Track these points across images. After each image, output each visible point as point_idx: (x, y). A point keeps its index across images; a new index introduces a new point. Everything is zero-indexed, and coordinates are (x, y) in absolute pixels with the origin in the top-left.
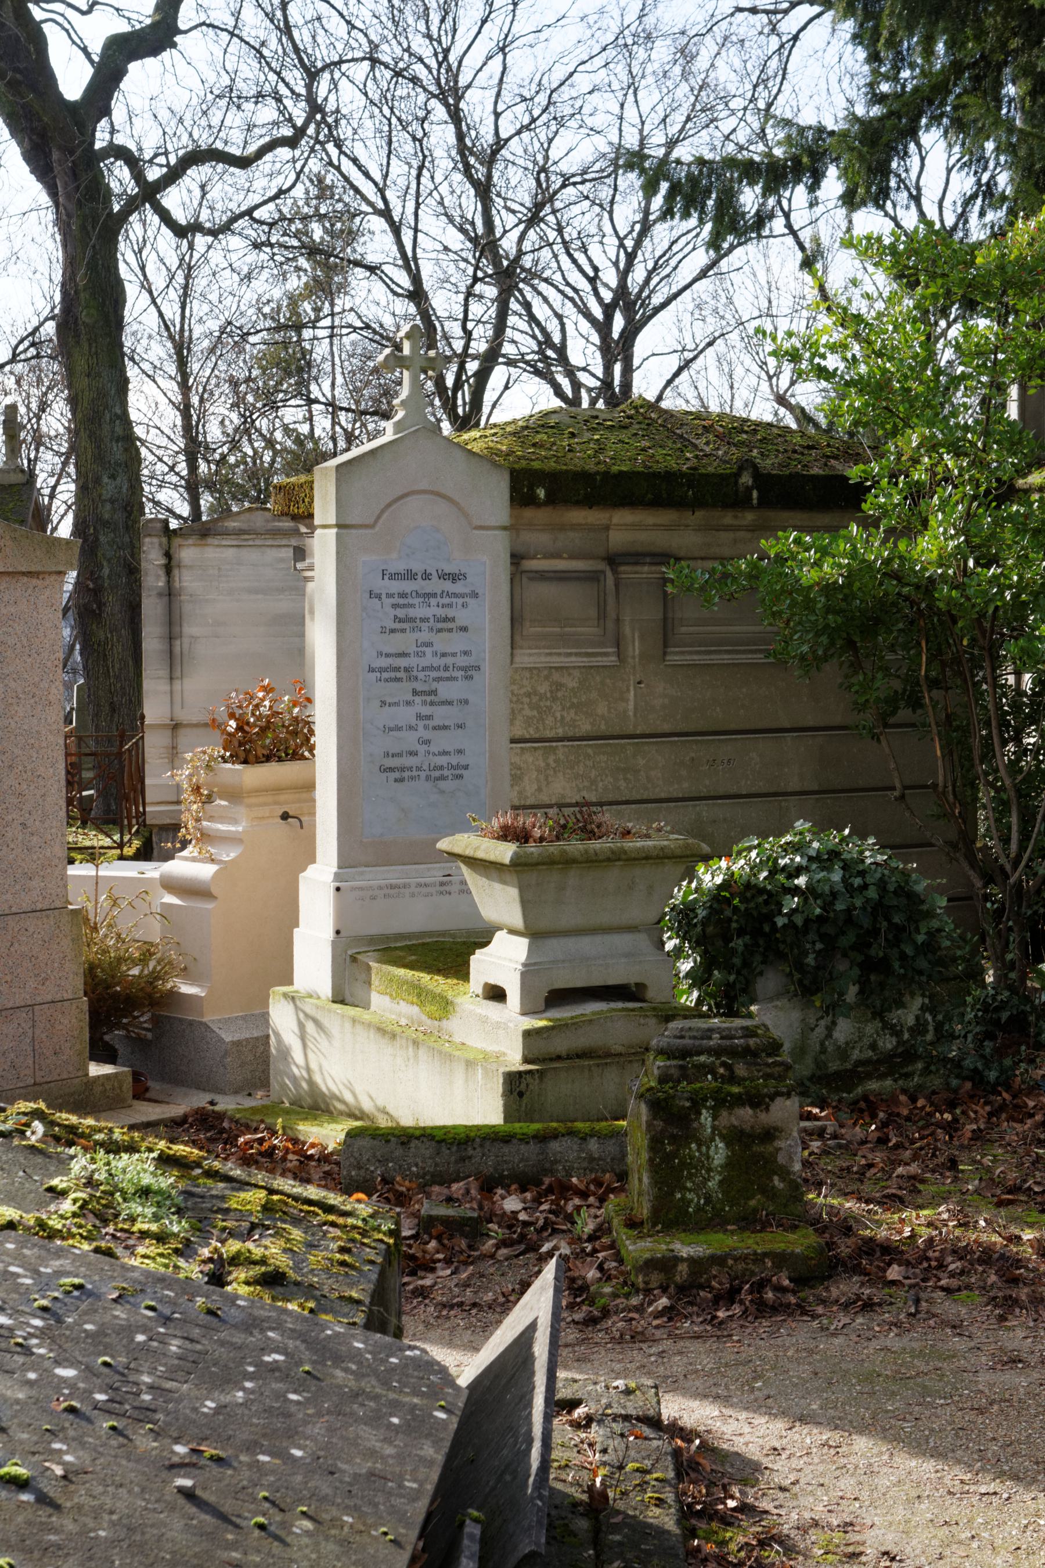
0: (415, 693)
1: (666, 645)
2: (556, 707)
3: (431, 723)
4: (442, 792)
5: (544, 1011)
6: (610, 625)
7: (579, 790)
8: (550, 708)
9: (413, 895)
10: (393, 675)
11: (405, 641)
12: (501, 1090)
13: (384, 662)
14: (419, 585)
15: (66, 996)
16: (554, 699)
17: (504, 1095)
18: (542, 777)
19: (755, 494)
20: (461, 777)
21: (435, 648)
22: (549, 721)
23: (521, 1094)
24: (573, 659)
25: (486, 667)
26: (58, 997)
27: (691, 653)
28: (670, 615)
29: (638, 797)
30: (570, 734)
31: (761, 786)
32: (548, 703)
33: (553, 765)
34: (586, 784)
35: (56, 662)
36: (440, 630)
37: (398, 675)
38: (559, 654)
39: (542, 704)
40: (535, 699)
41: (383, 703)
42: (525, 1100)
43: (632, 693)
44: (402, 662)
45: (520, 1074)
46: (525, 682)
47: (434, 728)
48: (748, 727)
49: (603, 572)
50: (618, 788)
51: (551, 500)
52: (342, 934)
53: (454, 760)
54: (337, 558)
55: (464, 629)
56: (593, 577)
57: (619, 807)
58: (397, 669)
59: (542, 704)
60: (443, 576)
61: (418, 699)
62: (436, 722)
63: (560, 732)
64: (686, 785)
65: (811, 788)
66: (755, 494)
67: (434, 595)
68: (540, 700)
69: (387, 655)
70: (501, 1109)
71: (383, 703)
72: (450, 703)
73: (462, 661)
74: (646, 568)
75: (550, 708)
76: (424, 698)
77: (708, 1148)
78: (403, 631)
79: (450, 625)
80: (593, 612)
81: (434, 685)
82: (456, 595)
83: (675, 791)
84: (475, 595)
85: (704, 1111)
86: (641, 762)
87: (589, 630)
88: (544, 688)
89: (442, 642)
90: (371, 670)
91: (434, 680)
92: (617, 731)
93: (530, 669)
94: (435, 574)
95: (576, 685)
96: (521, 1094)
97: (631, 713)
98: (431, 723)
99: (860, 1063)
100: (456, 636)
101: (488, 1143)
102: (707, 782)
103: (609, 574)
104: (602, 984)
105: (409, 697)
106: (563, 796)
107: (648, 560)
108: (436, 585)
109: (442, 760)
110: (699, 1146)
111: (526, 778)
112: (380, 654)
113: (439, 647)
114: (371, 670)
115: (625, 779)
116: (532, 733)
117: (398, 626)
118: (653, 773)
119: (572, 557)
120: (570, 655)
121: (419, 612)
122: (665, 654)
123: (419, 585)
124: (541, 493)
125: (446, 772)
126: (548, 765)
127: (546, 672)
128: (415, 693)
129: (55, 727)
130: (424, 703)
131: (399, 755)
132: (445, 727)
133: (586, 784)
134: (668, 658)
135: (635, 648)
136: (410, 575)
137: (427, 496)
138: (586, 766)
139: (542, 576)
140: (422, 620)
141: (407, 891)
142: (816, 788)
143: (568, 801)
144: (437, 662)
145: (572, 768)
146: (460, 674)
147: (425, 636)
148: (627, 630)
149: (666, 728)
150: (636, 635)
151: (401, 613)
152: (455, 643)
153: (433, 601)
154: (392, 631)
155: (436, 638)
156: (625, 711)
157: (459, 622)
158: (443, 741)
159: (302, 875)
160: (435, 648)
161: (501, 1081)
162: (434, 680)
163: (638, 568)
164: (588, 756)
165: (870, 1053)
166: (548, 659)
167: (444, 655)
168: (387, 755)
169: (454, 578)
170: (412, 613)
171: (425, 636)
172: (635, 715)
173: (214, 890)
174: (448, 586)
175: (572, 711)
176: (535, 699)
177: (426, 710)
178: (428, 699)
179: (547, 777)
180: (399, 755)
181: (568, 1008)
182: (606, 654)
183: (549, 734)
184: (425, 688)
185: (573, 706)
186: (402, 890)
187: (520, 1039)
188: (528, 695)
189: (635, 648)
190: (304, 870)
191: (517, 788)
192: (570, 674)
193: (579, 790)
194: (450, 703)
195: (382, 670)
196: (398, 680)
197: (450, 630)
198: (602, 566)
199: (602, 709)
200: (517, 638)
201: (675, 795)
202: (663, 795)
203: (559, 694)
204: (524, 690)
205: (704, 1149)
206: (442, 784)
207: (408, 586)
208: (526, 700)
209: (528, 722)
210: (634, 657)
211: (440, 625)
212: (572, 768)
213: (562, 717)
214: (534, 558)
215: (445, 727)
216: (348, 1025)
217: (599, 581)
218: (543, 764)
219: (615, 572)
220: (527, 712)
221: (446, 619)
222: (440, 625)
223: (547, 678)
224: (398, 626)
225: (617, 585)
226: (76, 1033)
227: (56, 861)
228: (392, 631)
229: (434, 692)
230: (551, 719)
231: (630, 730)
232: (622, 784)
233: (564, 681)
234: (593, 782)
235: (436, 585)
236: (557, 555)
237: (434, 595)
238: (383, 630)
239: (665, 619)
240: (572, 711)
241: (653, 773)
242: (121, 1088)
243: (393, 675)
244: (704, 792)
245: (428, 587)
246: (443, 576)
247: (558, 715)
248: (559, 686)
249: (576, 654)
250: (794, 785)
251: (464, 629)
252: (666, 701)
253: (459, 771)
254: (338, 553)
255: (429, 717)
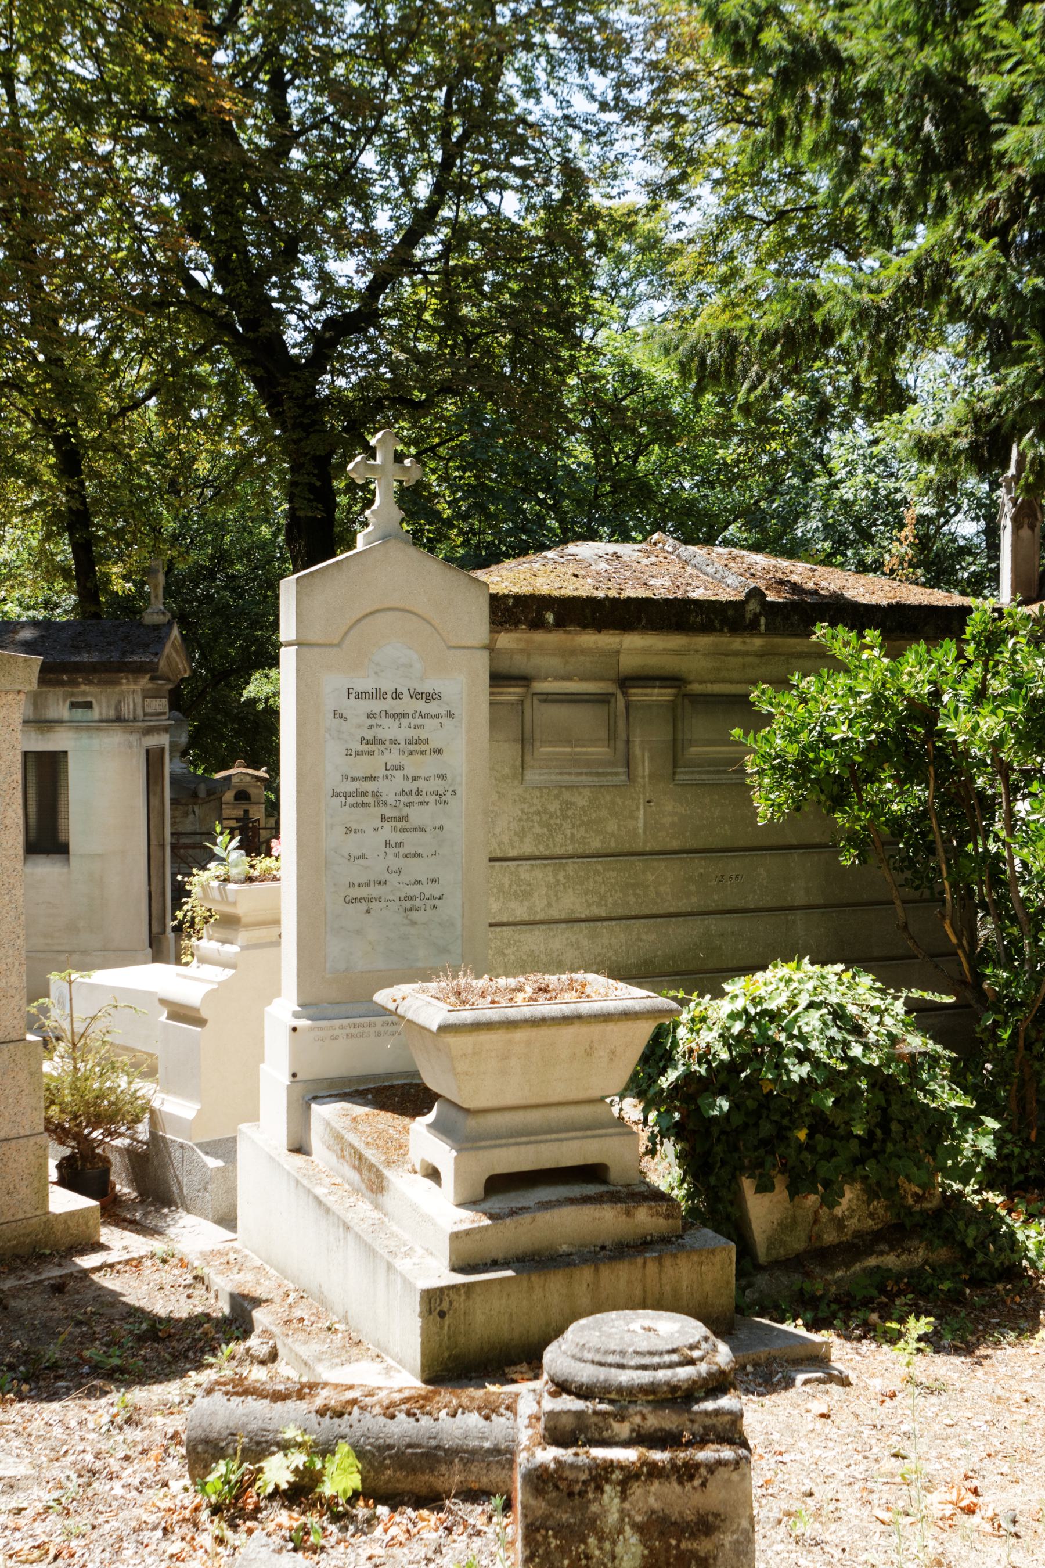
0: (384, 819)
1: (675, 765)
2: (567, 825)
3: (402, 851)
4: (413, 923)
5: (484, 1200)
6: (621, 745)
7: (589, 906)
8: (560, 826)
9: (379, 1034)
10: (359, 800)
11: (373, 764)
12: (418, 1309)
13: (350, 786)
14: (389, 705)
15: (22, 1133)
16: (565, 817)
17: (422, 1315)
18: (551, 893)
19: (763, 620)
20: (435, 907)
21: (405, 772)
22: (559, 838)
23: (442, 1314)
24: (584, 778)
25: (462, 791)
26: (13, 1134)
27: (699, 773)
28: (680, 736)
29: (648, 912)
30: (580, 851)
31: (768, 901)
32: (558, 821)
33: (563, 881)
34: (596, 899)
35: (14, 785)
36: (412, 753)
37: (366, 800)
38: (570, 774)
39: (552, 822)
40: (545, 817)
41: (349, 830)
42: (447, 1320)
43: (642, 812)
44: (369, 786)
45: (441, 1291)
46: (535, 801)
47: (405, 856)
48: (756, 844)
49: (614, 694)
50: (628, 903)
51: (560, 624)
52: (297, 1079)
53: (428, 890)
54: (297, 677)
55: (438, 751)
56: (603, 700)
57: (628, 922)
58: (364, 794)
59: (552, 822)
60: (415, 695)
61: (387, 826)
62: (407, 850)
63: (570, 849)
64: (694, 900)
65: (817, 902)
66: (763, 620)
67: (406, 715)
68: (551, 817)
69: (353, 779)
70: (418, 1331)
71: (349, 830)
72: (421, 829)
73: (437, 785)
74: (656, 691)
75: (560, 826)
76: (394, 824)
77: (614, 1543)
78: (371, 753)
79: (423, 747)
80: (603, 734)
81: (406, 811)
82: (429, 716)
83: (683, 905)
84: (451, 715)
85: (607, 1488)
86: (651, 878)
87: (599, 751)
88: (554, 807)
89: (413, 765)
90: (336, 794)
91: (405, 805)
92: (626, 847)
93: (540, 788)
94: (406, 693)
95: (586, 804)
96: (442, 1314)
97: (641, 831)
98: (402, 851)
99: (858, 1234)
100: (429, 758)
101: (836, 789)
102: (716, 897)
103: (620, 696)
104: (553, 1166)
105: (378, 823)
106: (573, 912)
107: (658, 683)
108: (408, 705)
109: (415, 890)
110: (601, 1539)
111: (536, 895)
112: (345, 777)
113: (410, 771)
114: (336, 794)
115: (635, 894)
116: (542, 850)
117: (364, 747)
118: (662, 889)
119: (583, 679)
120: (581, 774)
121: (390, 730)
122: (674, 773)
123: (389, 705)
124: (550, 617)
125: (417, 903)
126: (558, 881)
127: (556, 792)
128: (384, 819)
129: (12, 852)
130: (394, 829)
131: (367, 884)
132: (417, 855)
133: (596, 899)
134: (677, 777)
135: (644, 767)
136: (379, 695)
137: (397, 613)
138: (596, 882)
139: (548, 698)
140: (393, 742)
141: (372, 1030)
142: (822, 902)
143: (578, 915)
144: (408, 786)
145: (582, 884)
146: (432, 799)
147: (394, 757)
148: (637, 751)
149: (675, 844)
150: (647, 755)
151: (369, 735)
152: (428, 766)
153: (405, 722)
154: (359, 753)
155: (409, 762)
156: (635, 829)
157: (433, 744)
158: (416, 869)
159: (267, 1009)
160: (405, 772)
161: (418, 1299)
162: (405, 805)
163: (648, 691)
164: (597, 872)
165: (870, 1222)
166: (559, 777)
167: (416, 778)
168: (352, 885)
169: (429, 697)
170: (381, 734)
171: (394, 757)
172: (645, 832)
173: (204, 1014)
174: (421, 705)
175: (583, 829)
176: (545, 817)
177: (398, 837)
178: (399, 825)
179: (557, 892)
180: (367, 884)
181: (513, 1195)
182: (616, 774)
183: (559, 851)
184: (395, 813)
185: (583, 823)
186: (367, 1029)
187: (447, 1241)
188: (538, 813)
189: (644, 767)
190: (269, 1003)
191: (526, 904)
192: (580, 794)
193: (589, 906)
194: (421, 829)
195: (346, 795)
196: (365, 805)
197: (423, 753)
198: (609, 687)
199: (612, 826)
200: (528, 758)
201: (684, 909)
202: (672, 910)
203: (570, 813)
204: (534, 808)
205: (607, 1545)
206: (414, 915)
207: (377, 706)
208: (536, 818)
209: (538, 838)
210: (644, 777)
211: (412, 747)
212: (582, 884)
213: (573, 835)
214: (545, 679)
215: (417, 855)
216: (293, 1184)
217: (609, 702)
218: (552, 880)
219: (625, 694)
220: (538, 830)
221: (419, 741)
222: (412, 747)
223: (557, 797)
224: (364, 747)
225: (627, 707)
226: (33, 1171)
227: (12, 992)
228: (359, 753)
229: (405, 818)
230: (561, 836)
231: (639, 847)
232: (632, 899)
233: (574, 799)
234: (602, 897)
235: (408, 705)
236: (568, 678)
237: (406, 715)
238: (349, 752)
239: (675, 740)
240: (583, 829)
241: (662, 889)
242: (86, 1224)
243: (359, 800)
244: (712, 906)
245: (397, 706)
246: (415, 695)
247: (568, 832)
248: (570, 804)
249: (586, 774)
250: (801, 899)
251: (438, 751)
252: (676, 819)
253: (434, 901)
254: (298, 670)
255: (399, 845)
